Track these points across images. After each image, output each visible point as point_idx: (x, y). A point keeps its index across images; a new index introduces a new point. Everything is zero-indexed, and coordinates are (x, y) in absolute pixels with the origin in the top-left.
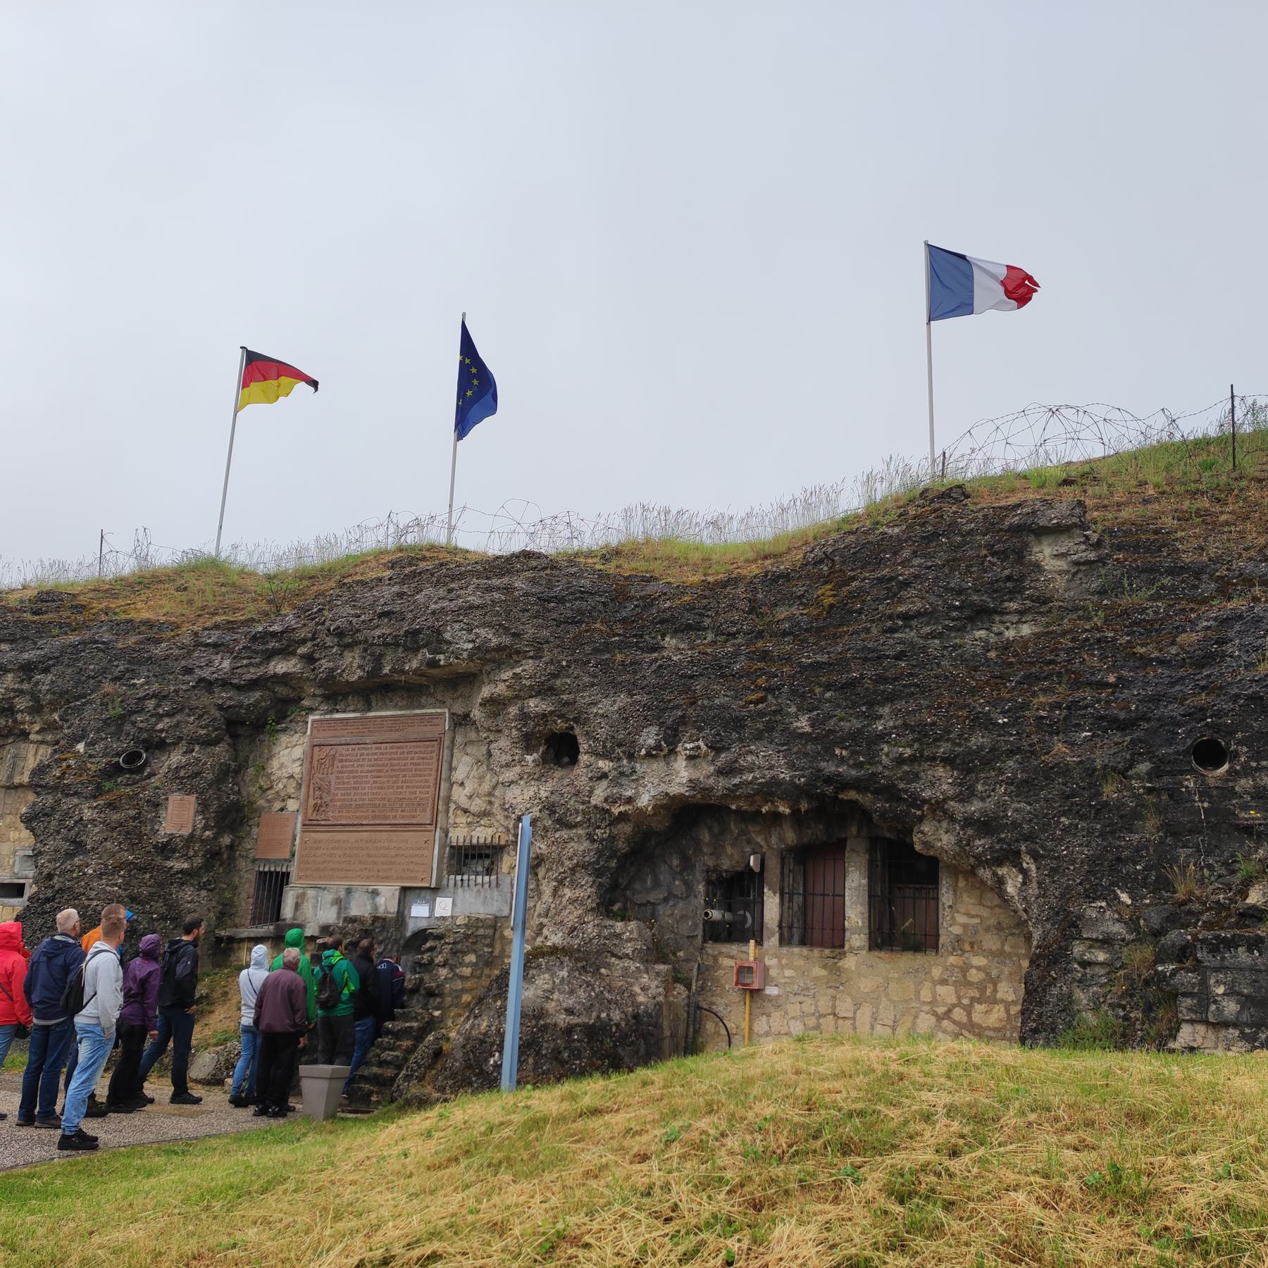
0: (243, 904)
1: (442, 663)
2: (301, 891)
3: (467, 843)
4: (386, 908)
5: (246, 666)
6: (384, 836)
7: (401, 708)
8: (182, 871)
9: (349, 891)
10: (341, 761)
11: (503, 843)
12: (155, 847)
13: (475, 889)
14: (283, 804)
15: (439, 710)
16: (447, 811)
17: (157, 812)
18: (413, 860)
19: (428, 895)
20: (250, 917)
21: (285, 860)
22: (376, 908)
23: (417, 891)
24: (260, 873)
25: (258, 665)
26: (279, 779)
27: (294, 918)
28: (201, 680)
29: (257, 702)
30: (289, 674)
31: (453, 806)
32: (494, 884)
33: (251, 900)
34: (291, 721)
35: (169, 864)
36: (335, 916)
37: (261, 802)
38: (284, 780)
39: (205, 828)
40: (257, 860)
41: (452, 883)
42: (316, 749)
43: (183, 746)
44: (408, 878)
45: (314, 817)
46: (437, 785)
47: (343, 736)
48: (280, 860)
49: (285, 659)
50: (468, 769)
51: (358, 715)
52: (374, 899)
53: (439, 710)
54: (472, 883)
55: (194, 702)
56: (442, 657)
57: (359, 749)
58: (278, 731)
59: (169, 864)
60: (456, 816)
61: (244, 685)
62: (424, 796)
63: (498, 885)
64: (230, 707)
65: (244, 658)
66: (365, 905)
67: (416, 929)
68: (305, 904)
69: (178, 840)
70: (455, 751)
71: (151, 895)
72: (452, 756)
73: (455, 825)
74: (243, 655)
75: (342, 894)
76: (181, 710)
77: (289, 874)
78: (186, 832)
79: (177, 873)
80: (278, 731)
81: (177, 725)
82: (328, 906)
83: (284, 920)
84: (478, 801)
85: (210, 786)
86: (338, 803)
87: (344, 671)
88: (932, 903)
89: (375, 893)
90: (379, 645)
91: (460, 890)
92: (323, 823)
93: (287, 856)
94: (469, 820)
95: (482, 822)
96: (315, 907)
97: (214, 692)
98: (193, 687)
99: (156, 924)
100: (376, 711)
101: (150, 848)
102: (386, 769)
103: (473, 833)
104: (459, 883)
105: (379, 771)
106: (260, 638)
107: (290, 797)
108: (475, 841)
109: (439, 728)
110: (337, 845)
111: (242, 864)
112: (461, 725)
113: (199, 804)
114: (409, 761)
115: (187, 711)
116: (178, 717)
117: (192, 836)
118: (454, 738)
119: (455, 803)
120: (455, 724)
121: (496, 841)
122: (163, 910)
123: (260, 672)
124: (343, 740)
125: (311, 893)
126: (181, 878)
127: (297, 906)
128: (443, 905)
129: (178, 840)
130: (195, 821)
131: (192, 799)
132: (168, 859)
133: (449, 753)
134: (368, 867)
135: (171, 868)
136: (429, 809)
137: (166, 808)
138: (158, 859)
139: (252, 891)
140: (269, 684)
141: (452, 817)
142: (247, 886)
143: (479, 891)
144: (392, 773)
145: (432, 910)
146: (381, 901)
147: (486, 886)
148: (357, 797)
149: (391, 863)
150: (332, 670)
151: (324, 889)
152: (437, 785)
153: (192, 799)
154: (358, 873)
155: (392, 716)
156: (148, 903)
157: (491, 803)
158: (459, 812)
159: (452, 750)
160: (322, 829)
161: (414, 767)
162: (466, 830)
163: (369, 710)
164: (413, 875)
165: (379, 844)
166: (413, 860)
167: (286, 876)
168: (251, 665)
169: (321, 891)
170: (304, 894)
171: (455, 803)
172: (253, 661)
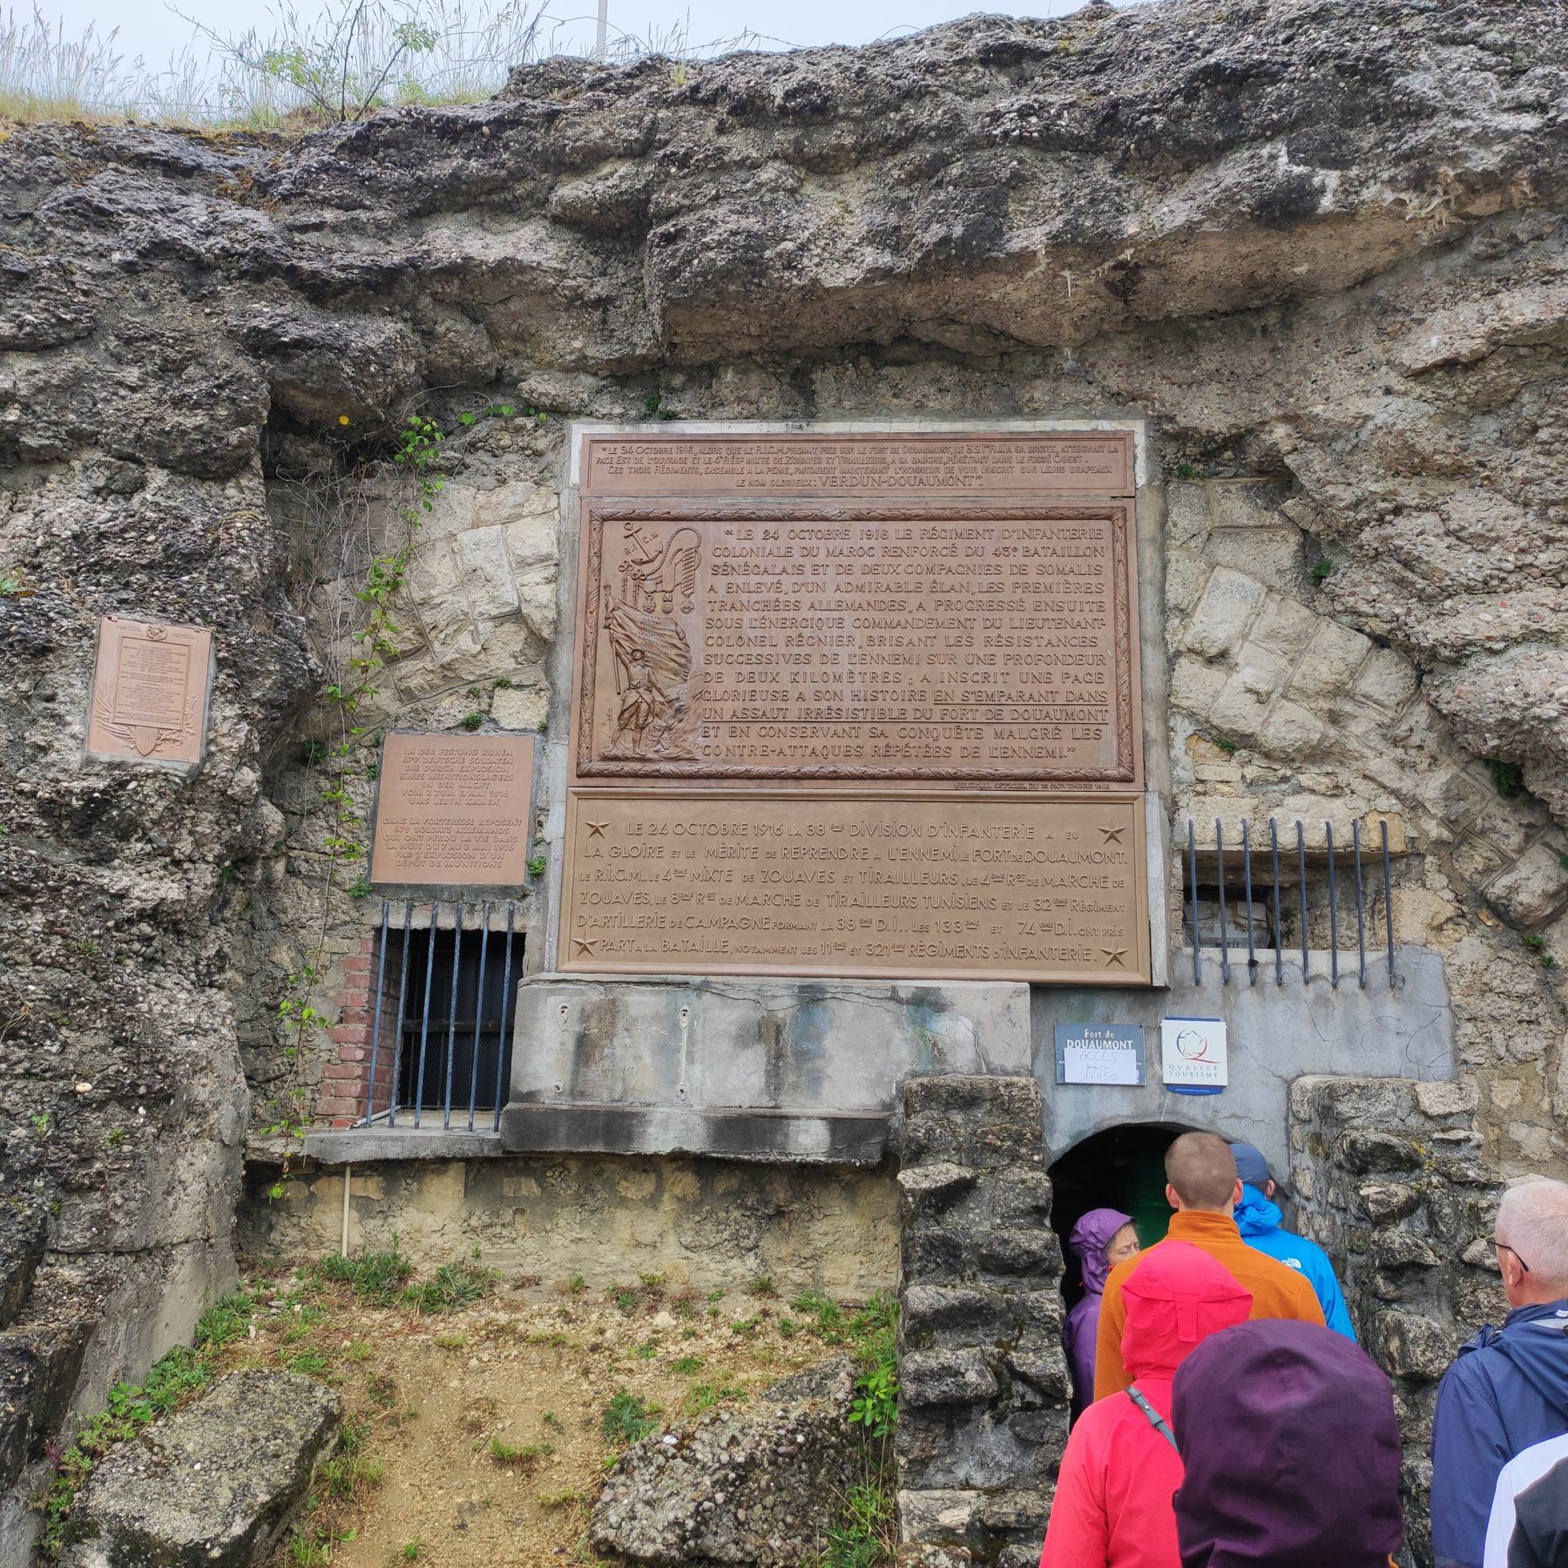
0: (322, 1040)
1: (1327, 203)
2: (595, 996)
3: (1259, 843)
4: (981, 1054)
5: (336, 229)
6: (933, 814)
7: (943, 415)
8: (153, 915)
9: (811, 996)
10: (726, 570)
11: (1396, 845)
12: (47, 809)
13: (1310, 993)
14: (474, 707)
15: (1105, 425)
16: (1168, 744)
17: (39, 678)
18: (1062, 894)
19: (1122, 1013)
20: (356, 1087)
21: (506, 891)
22: (937, 1053)
23: (1075, 1000)
24: (395, 936)
25: (383, 232)
26: (461, 621)
27: (575, 1092)
28: (161, 249)
29: (389, 350)
30: (523, 268)
31: (1183, 728)
32: (1378, 976)
33: (359, 1029)
34: (472, 447)
35: (114, 878)
36: (758, 1080)
37: (385, 700)
38: (485, 627)
39: (244, 757)
40: (378, 889)
41: (1211, 975)
42: (614, 531)
43: (89, 468)
44: (1067, 956)
45: (625, 746)
46: (1125, 651)
47: (722, 491)
48: (479, 891)
49: (481, 225)
50: (1244, 610)
51: (778, 427)
52: (922, 1023)
53: (1105, 425)
54: (1292, 973)
55: (134, 318)
56: (1331, 178)
57: (793, 535)
58: (431, 470)
59: (114, 878)
60: (1198, 760)
61: (347, 285)
62: (1084, 689)
63: (1395, 981)
64: (301, 344)
65: (325, 203)
66: (887, 1044)
67: (1089, 1128)
68: (622, 1039)
69: (149, 786)
70: (1173, 554)
71: (60, 1000)
72: (1164, 568)
73: (1201, 787)
74: (322, 192)
75: (784, 1006)
76: (86, 337)
77: (520, 938)
78: (180, 759)
79: (142, 915)
80: (431, 470)
81: (74, 384)
82: (726, 1046)
83: (530, 1096)
84: (1296, 711)
85: (249, 603)
86: (728, 708)
87: (803, 247)
88: (1154, 1038)
89: (926, 1004)
90: (1022, 141)
91: (1248, 998)
92: (667, 767)
93: (519, 878)
94: (1251, 772)
95: (1304, 780)
96: (666, 1050)
97: (214, 295)
98: (129, 268)
99: (95, 1119)
100: (842, 417)
101: (26, 813)
102: (913, 600)
103: (1276, 814)
104: (1242, 975)
105: (892, 606)
106: (387, 144)
107: (503, 684)
108: (1287, 839)
109: (1113, 480)
110: (731, 842)
111: (303, 903)
112: (1185, 474)
113: (221, 663)
114: (1007, 579)
115: (113, 343)
116: (75, 359)
117: (196, 778)
118: (1165, 515)
119: (1191, 715)
120: (1169, 472)
121: (1372, 839)
122: (114, 1062)
123: (395, 253)
124: (722, 504)
125: (640, 1002)
126: (147, 940)
127: (584, 1049)
128: (1192, 1045)
129: (149, 786)
130: (211, 724)
131: (199, 639)
132: (104, 858)
133: (1156, 558)
134: (874, 915)
135: (121, 896)
136: (1109, 733)
137: (89, 668)
138: (66, 861)
139: (359, 996)
140: (425, 301)
141: (1186, 761)
142: (333, 979)
143: (1321, 1000)
144: (942, 614)
145: (1149, 1058)
146: (954, 1030)
147: (1350, 984)
148: (808, 689)
149: (976, 905)
150: (756, 242)
151: (703, 988)
152: (1125, 651)
153: (199, 639)
154: (837, 937)
155: (922, 438)
156: (48, 1034)
157: (1334, 718)
158: (1203, 747)
159: (1162, 549)
160: (662, 787)
161: (1029, 598)
162: (1248, 802)
163: (811, 416)
164: (1068, 943)
165: (913, 843)
166: (1062, 894)
167: (508, 947)
168: (357, 228)
169: (685, 999)
170: (610, 1011)
171: (1191, 715)
172: (363, 215)
